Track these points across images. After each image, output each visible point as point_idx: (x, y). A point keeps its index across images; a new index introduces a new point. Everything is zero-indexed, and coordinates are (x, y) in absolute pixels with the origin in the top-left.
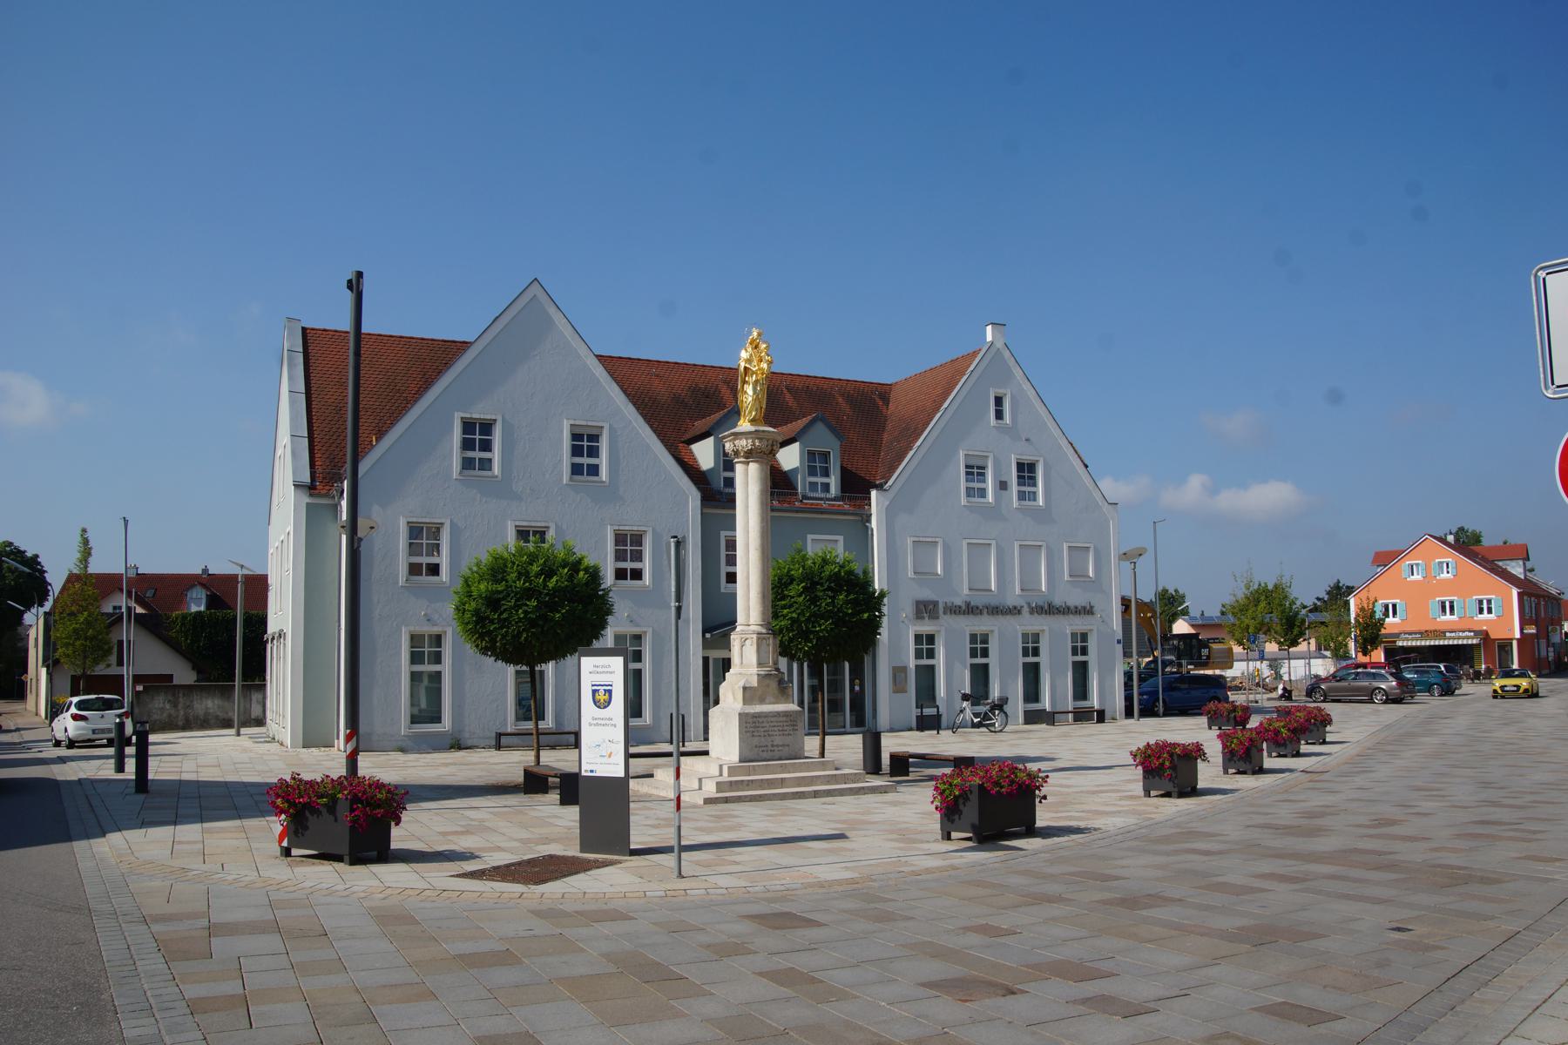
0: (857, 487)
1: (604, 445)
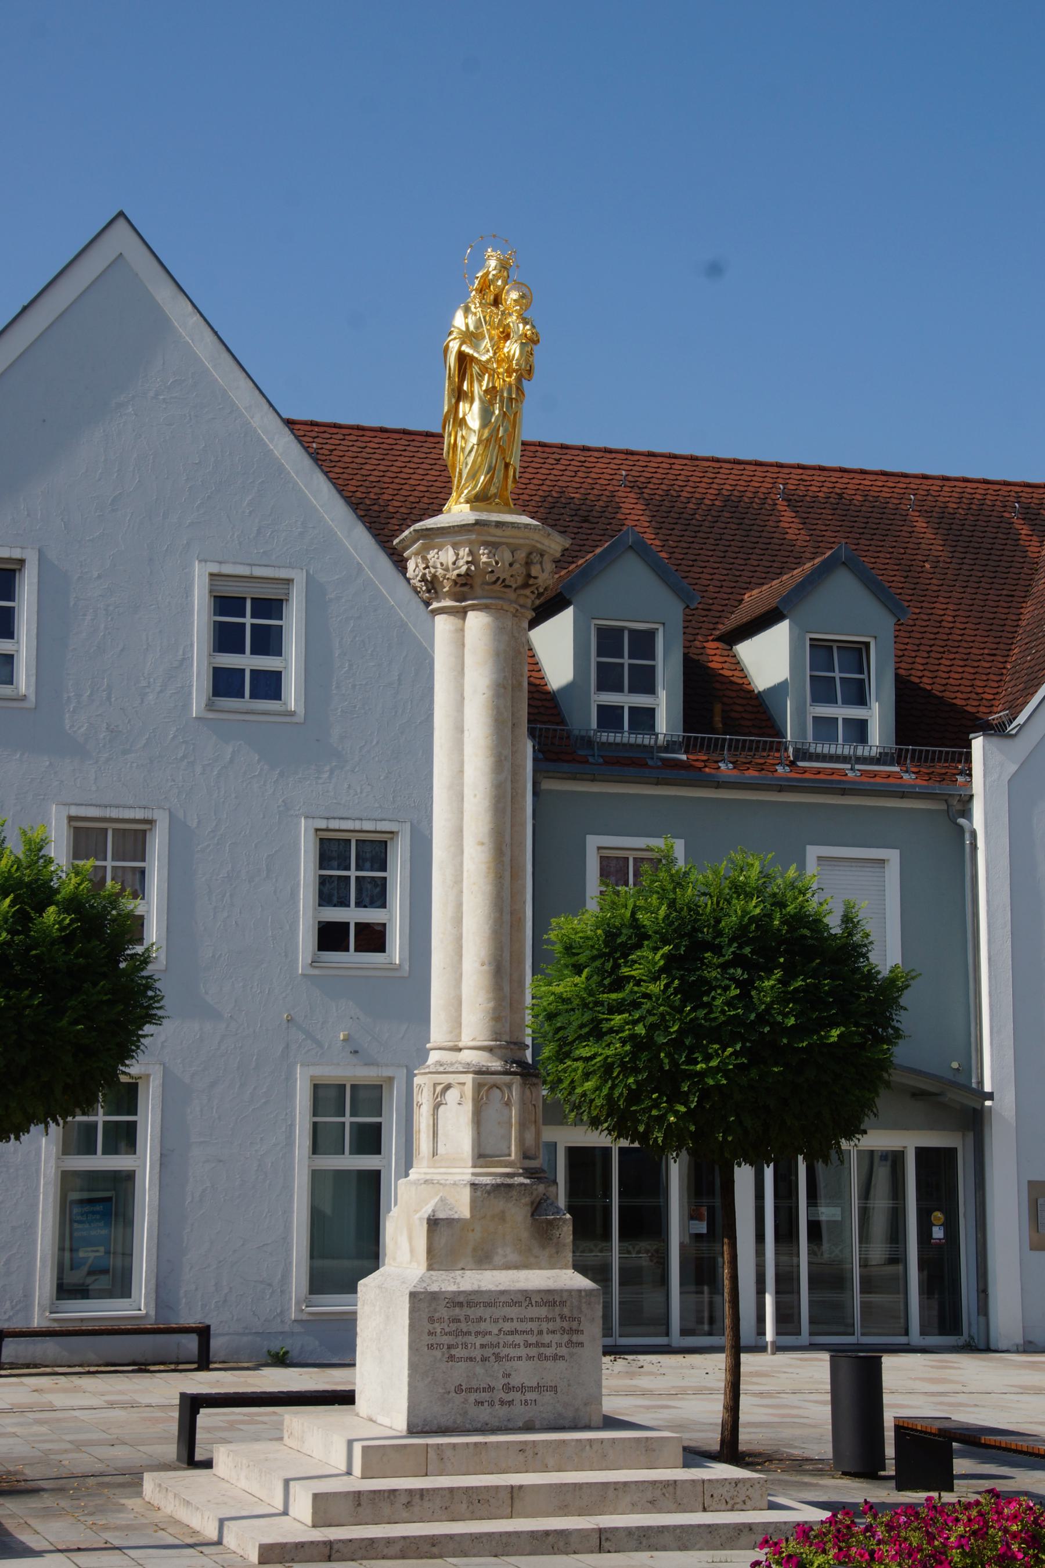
0: (935, 730)
1: (293, 625)
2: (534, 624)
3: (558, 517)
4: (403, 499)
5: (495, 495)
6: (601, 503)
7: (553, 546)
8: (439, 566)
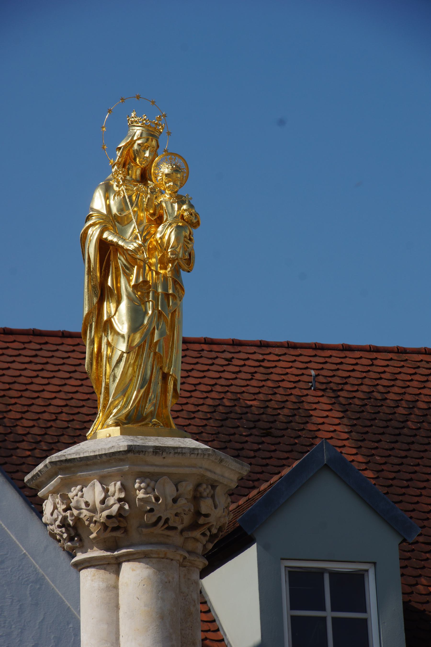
2: (205, 572)
3: (232, 431)
4: (36, 417)
5: (152, 414)
6: (286, 411)
7: (227, 474)
8: (83, 506)
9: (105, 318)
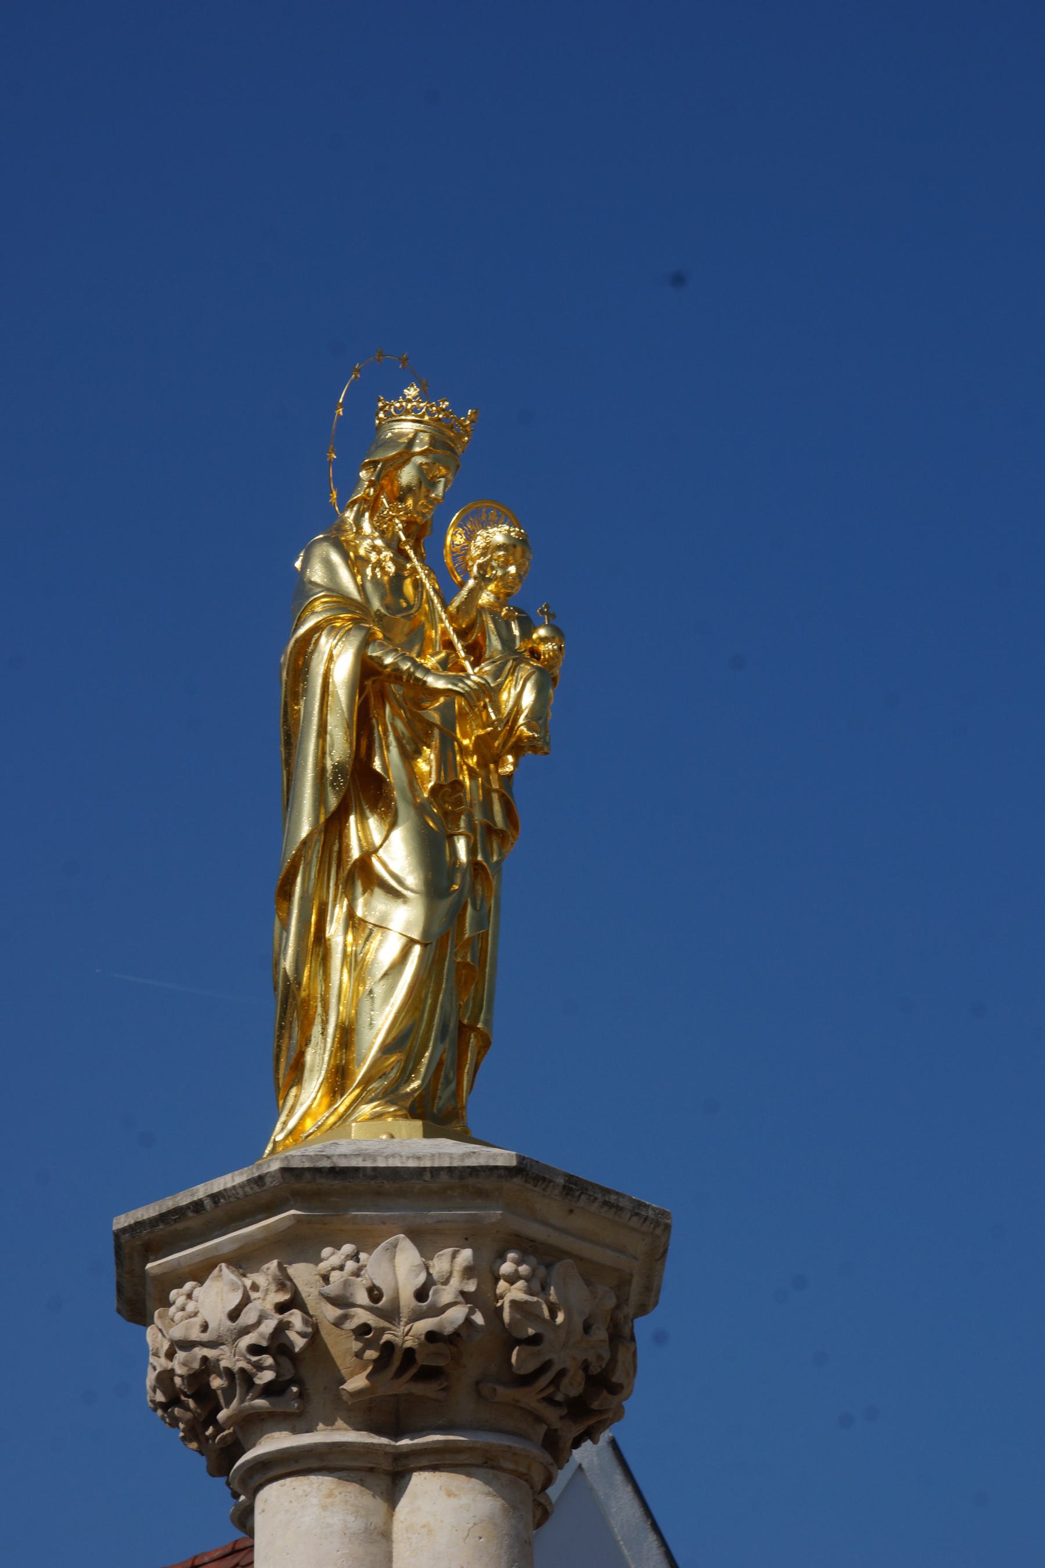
9: (355, 854)
